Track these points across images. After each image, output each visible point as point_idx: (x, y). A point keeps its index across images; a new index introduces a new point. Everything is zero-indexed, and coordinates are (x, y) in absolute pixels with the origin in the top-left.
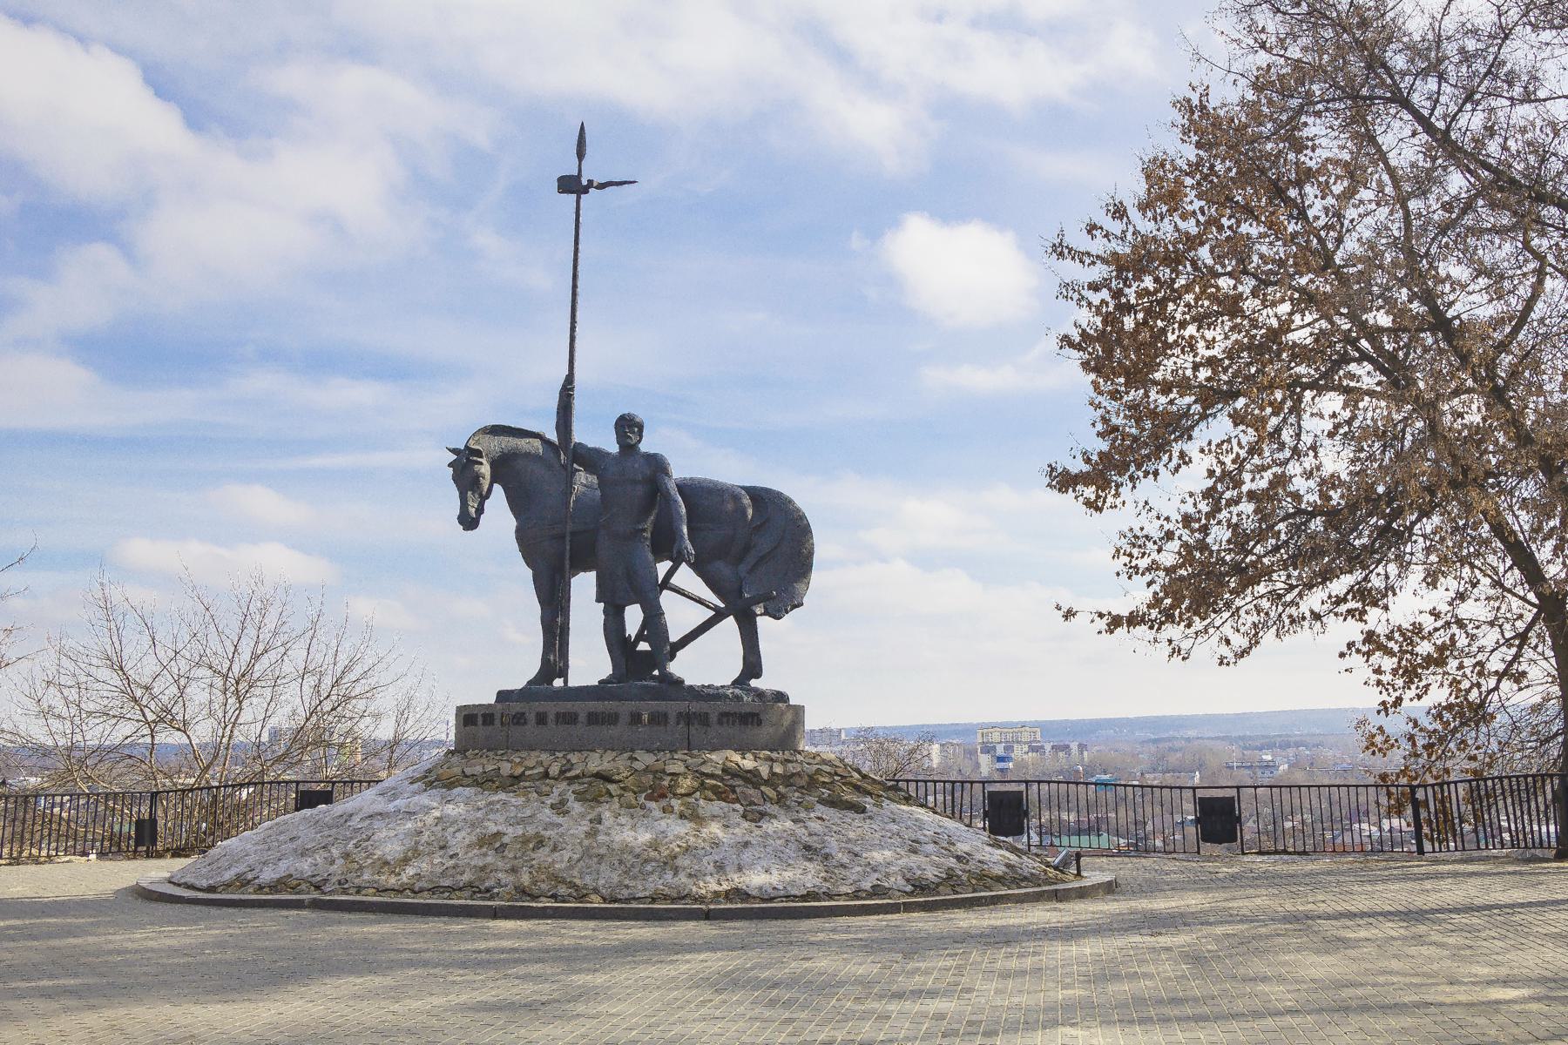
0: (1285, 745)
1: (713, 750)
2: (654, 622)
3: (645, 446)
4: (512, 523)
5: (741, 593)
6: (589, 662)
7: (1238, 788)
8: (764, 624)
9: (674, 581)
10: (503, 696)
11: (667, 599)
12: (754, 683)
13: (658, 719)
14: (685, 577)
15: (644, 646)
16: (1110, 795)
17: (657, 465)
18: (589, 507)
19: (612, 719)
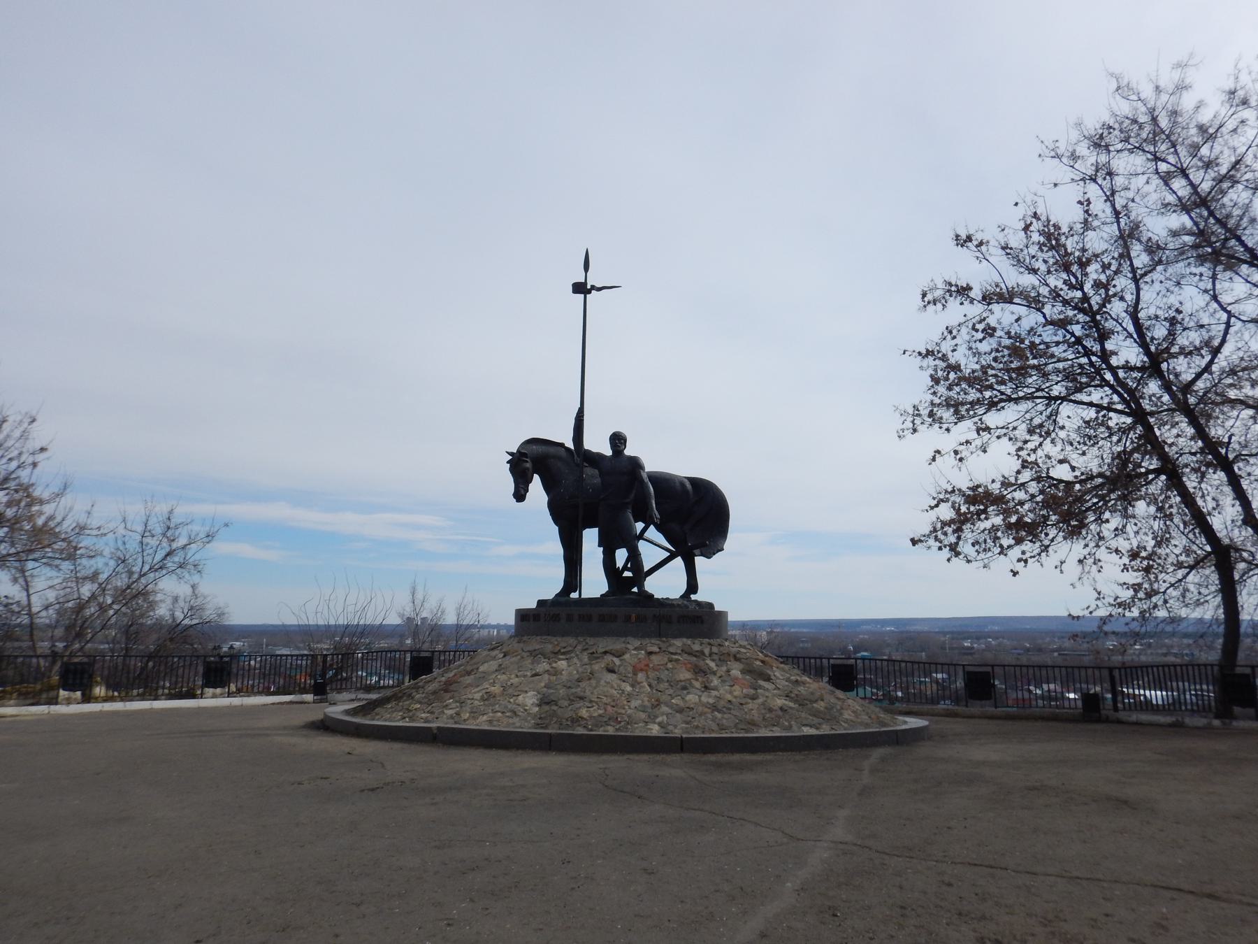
0: (978, 638)
1: (675, 637)
2: (634, 557)
3: (628, 452)
4: (545, 498)
5: (686, 543)
6: (594, 583)
7: (993, 666)
8: (700, 561)
9: (647, 535)
10: (541, 603)
11: (642, 545)
12: (693, 597)
13: (640, 619)
14: (652, 533)
15: (627, 574)
16: (1044, 672)
17: (635, 464)
18: (588, 487)
19: (613, 618)
